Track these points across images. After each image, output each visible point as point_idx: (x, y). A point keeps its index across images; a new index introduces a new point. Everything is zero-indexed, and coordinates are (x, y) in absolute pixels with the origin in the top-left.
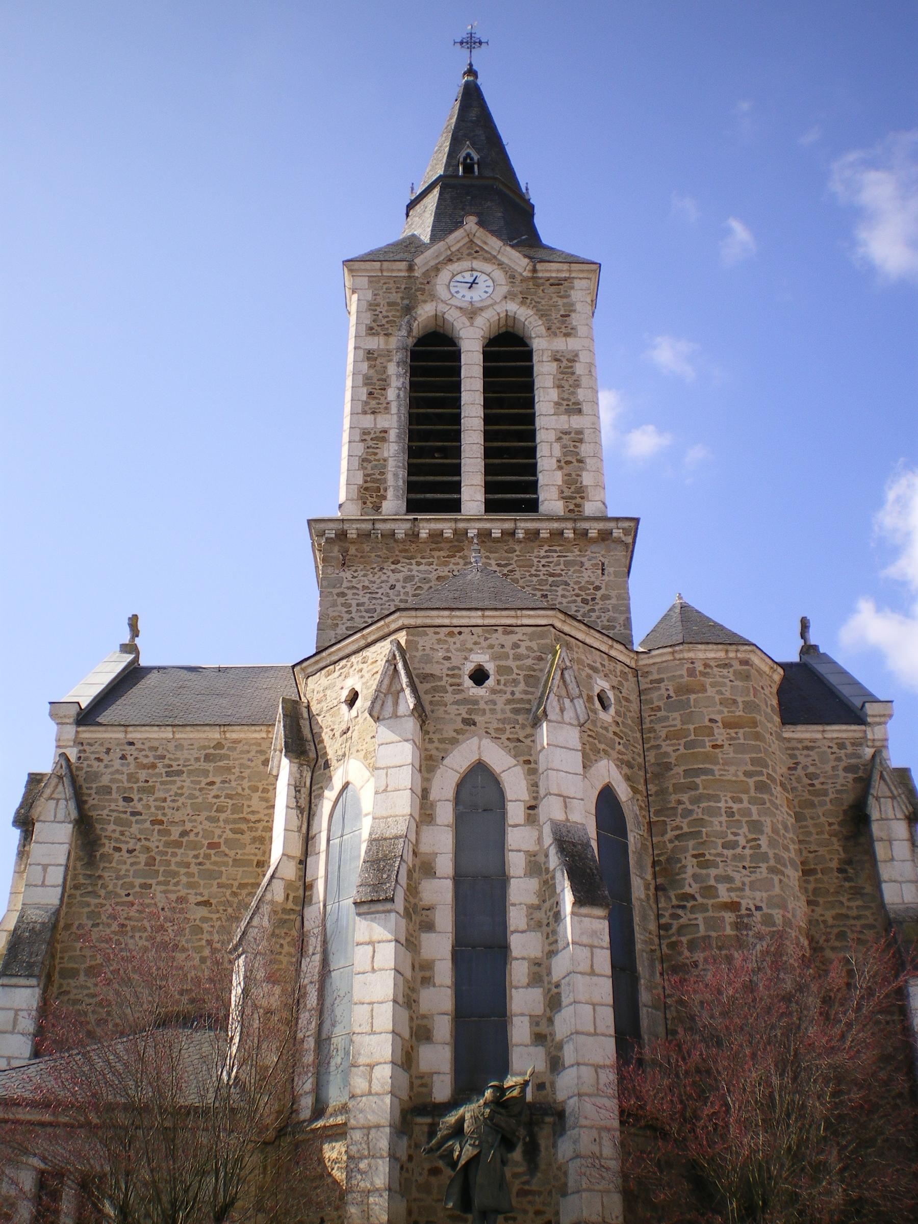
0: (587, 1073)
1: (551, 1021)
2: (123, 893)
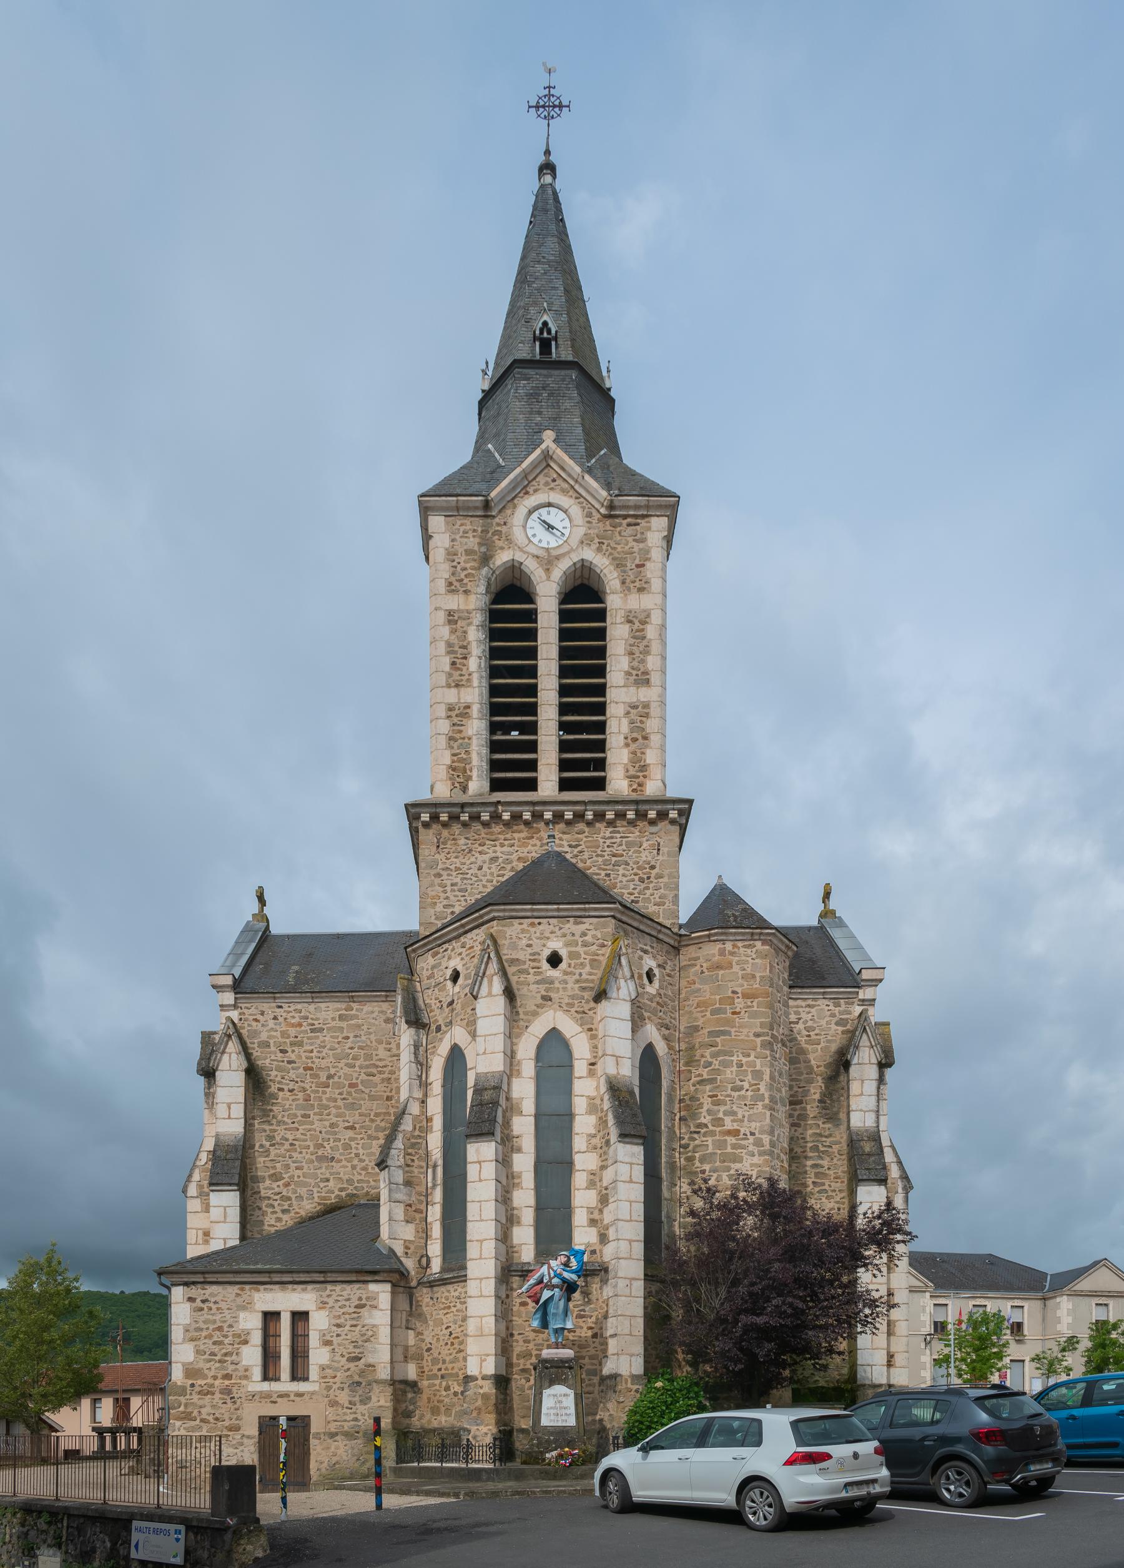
0: (624, 1245)
1: (601, 1211)
2: (290, 1121)
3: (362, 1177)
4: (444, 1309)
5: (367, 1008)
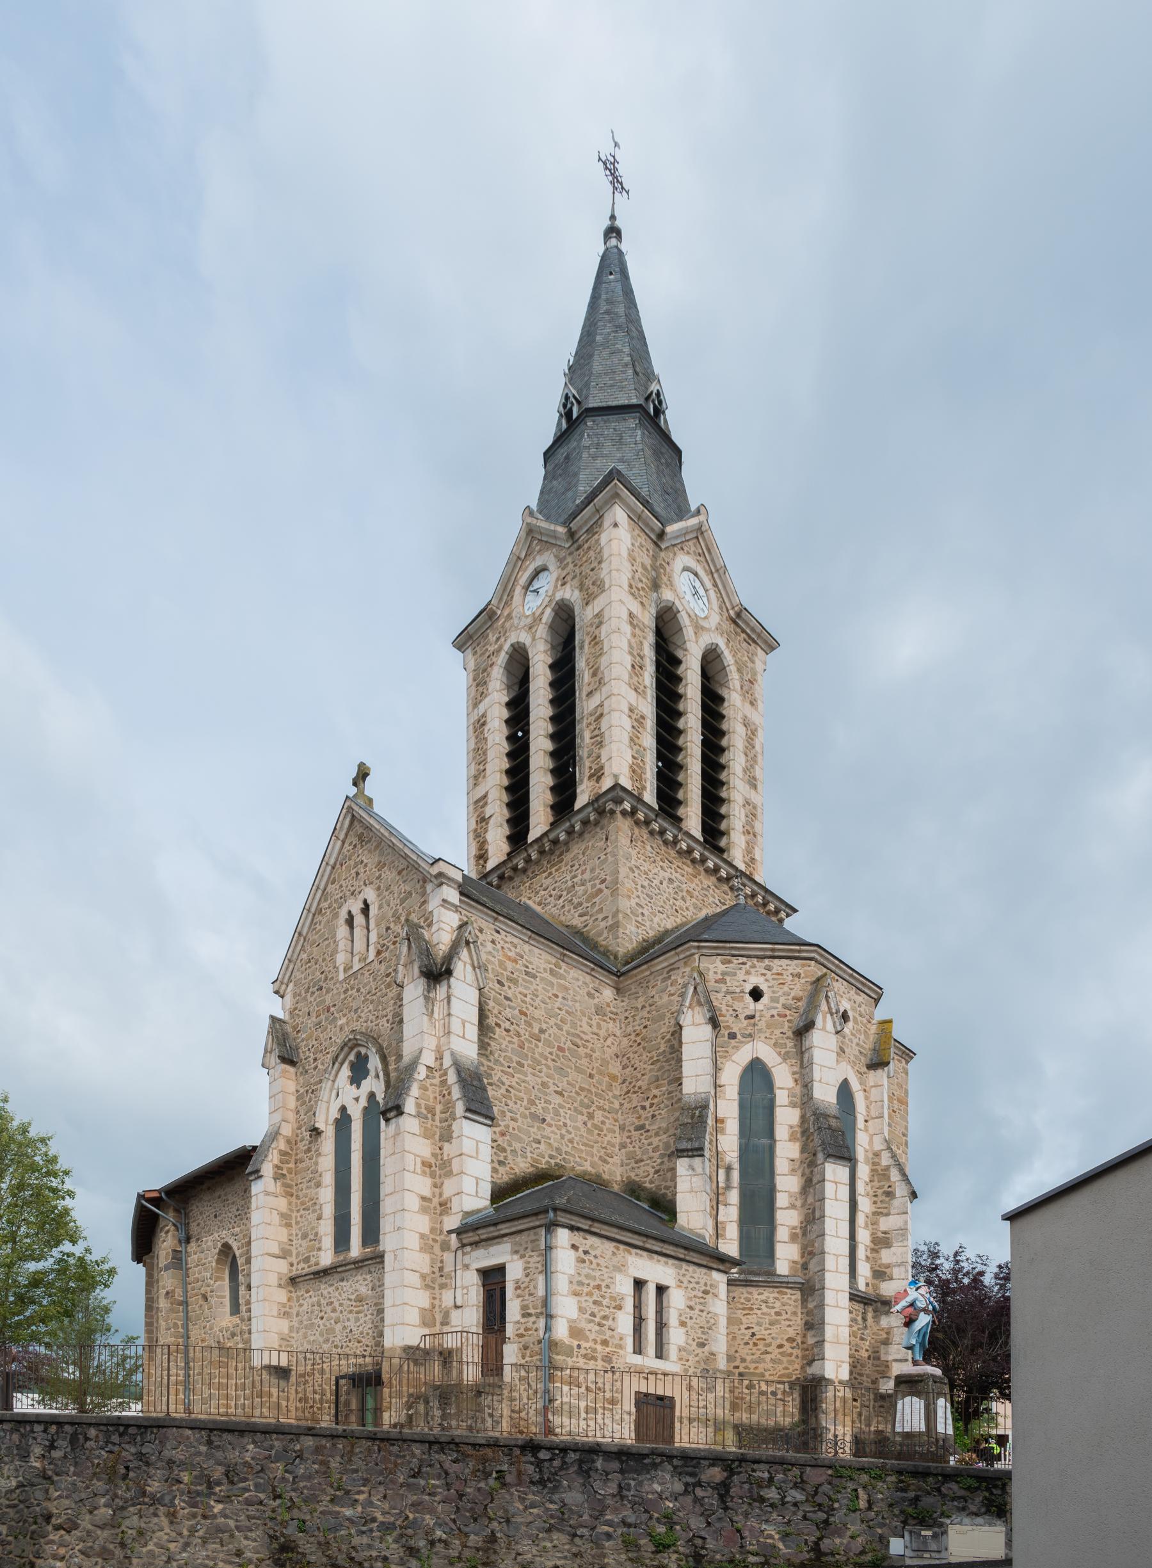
3: (569, 1150)
4: (744, 1309)
5: (574, 973)
